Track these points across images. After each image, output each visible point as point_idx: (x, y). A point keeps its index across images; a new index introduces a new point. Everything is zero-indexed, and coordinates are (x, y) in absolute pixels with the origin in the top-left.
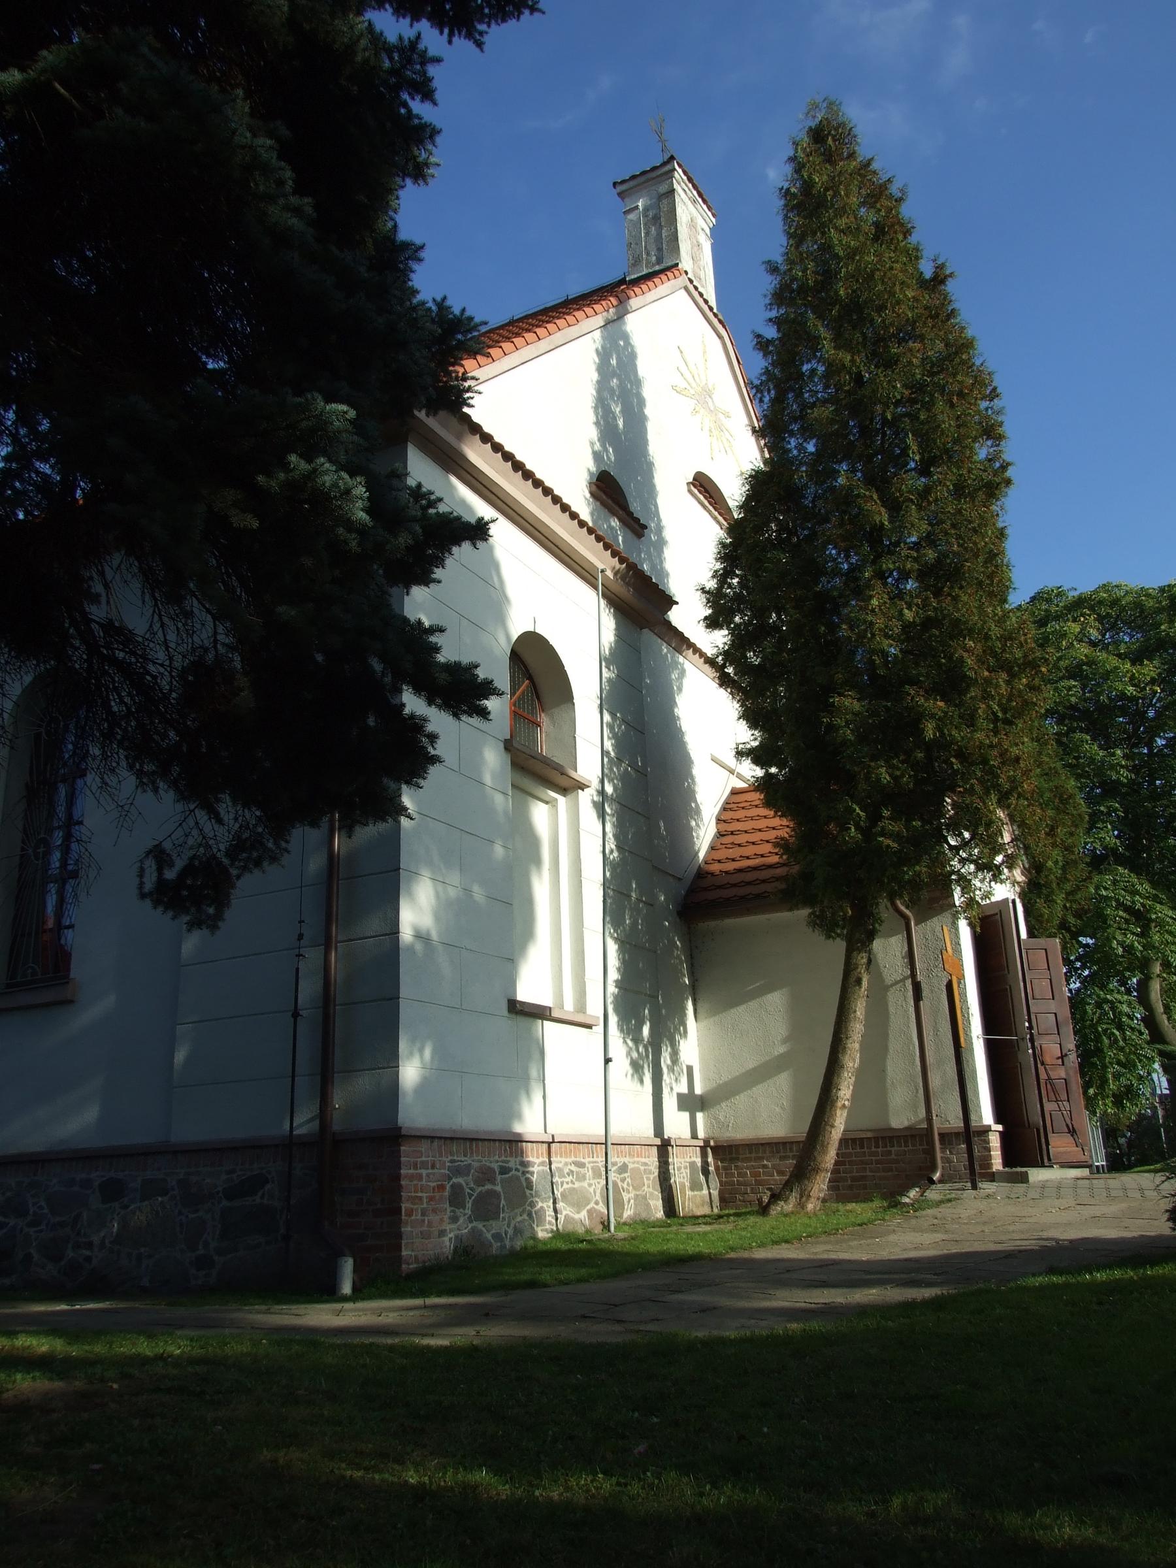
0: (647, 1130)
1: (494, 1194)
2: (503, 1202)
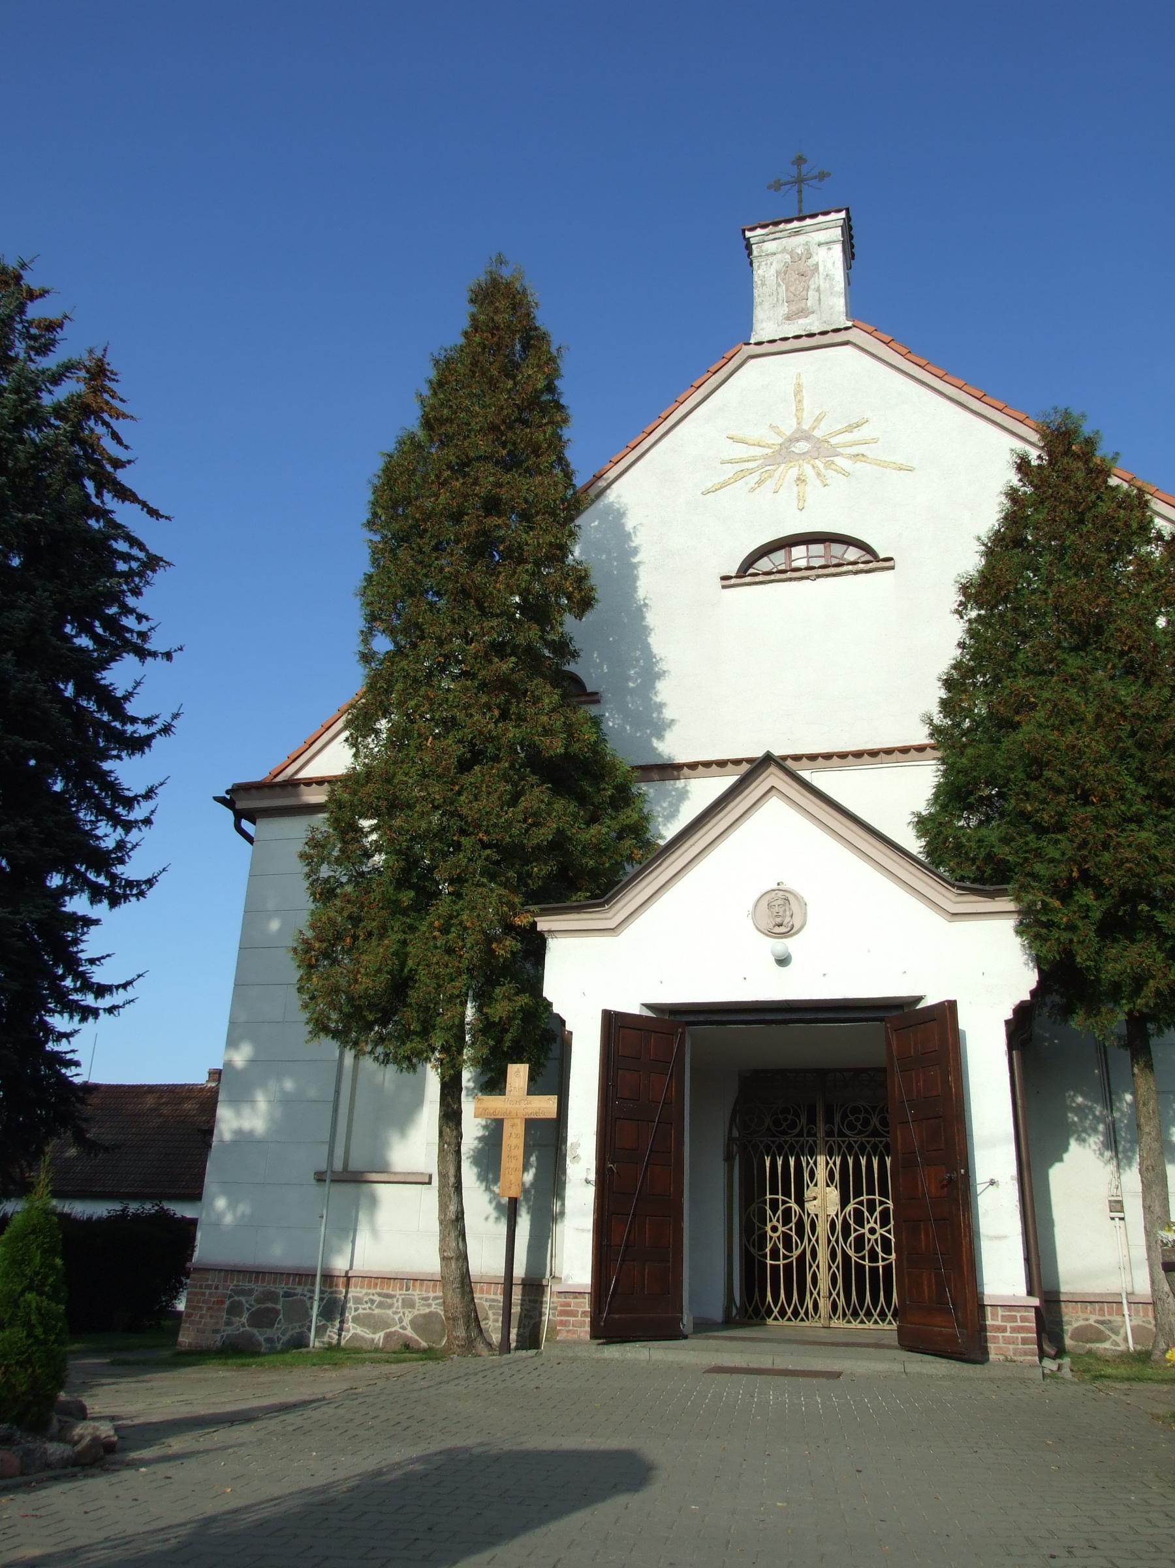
0: (501, 1271)
1: (277, 1312)
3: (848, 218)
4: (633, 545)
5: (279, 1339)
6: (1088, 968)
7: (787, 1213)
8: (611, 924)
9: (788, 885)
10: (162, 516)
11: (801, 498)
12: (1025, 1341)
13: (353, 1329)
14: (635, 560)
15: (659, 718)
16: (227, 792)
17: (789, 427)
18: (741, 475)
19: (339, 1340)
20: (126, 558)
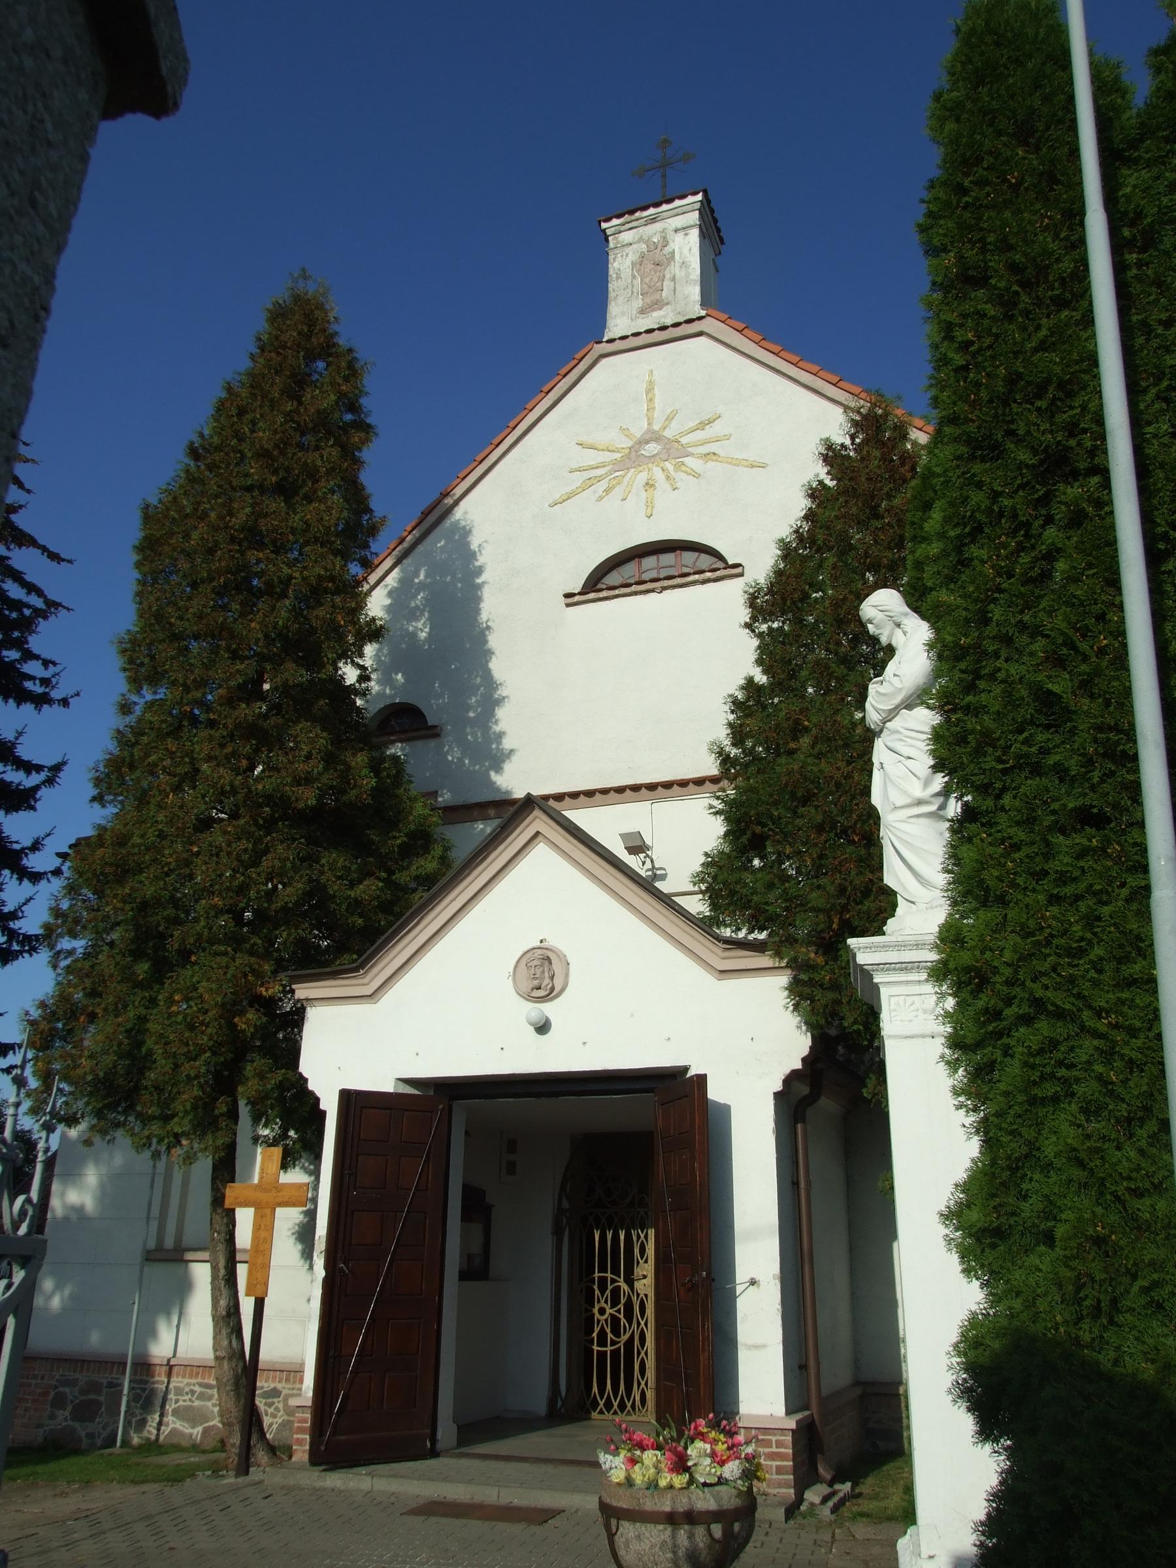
1: (98, 1404)
2: (103, 1409)
3: (707, 200)
4: (477, 564)
5: (99, 1434)
6: (858, 1032)
7: (616, 1292)
8: (368, 990)
9: (552, 942)
10: (64, 560)
11: (650, 504)
12: (779, 1470)
13: (173, 1423)
14: (479, 581)
15: (498, 748)
16: (70, 847)
17: (639, 429)
18: (590, 483)
19: (158, 1435)
20: (18, 605)
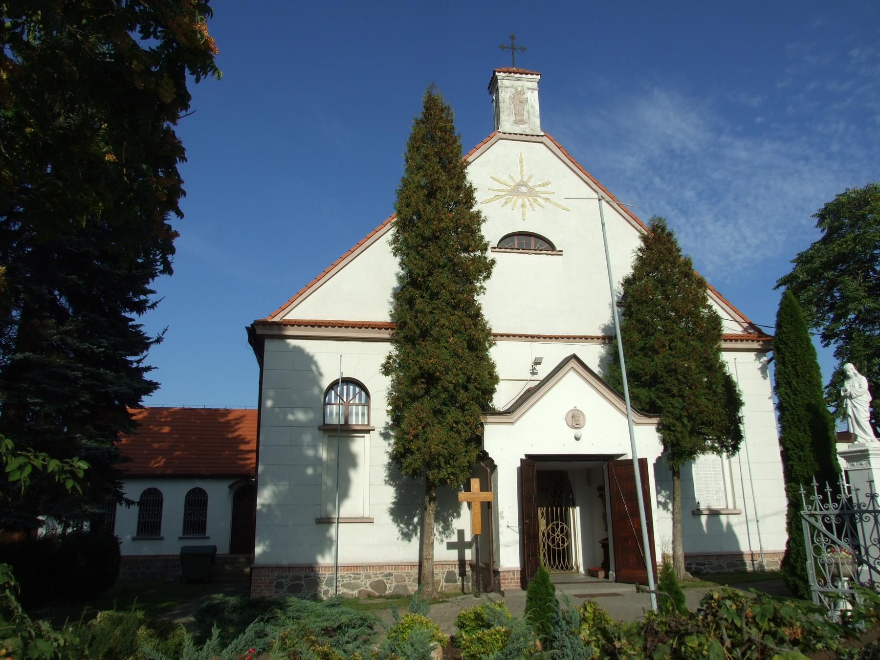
1: (302, 586)
11: (524, 214)
17: (518, 179)
18: (497, 197)
